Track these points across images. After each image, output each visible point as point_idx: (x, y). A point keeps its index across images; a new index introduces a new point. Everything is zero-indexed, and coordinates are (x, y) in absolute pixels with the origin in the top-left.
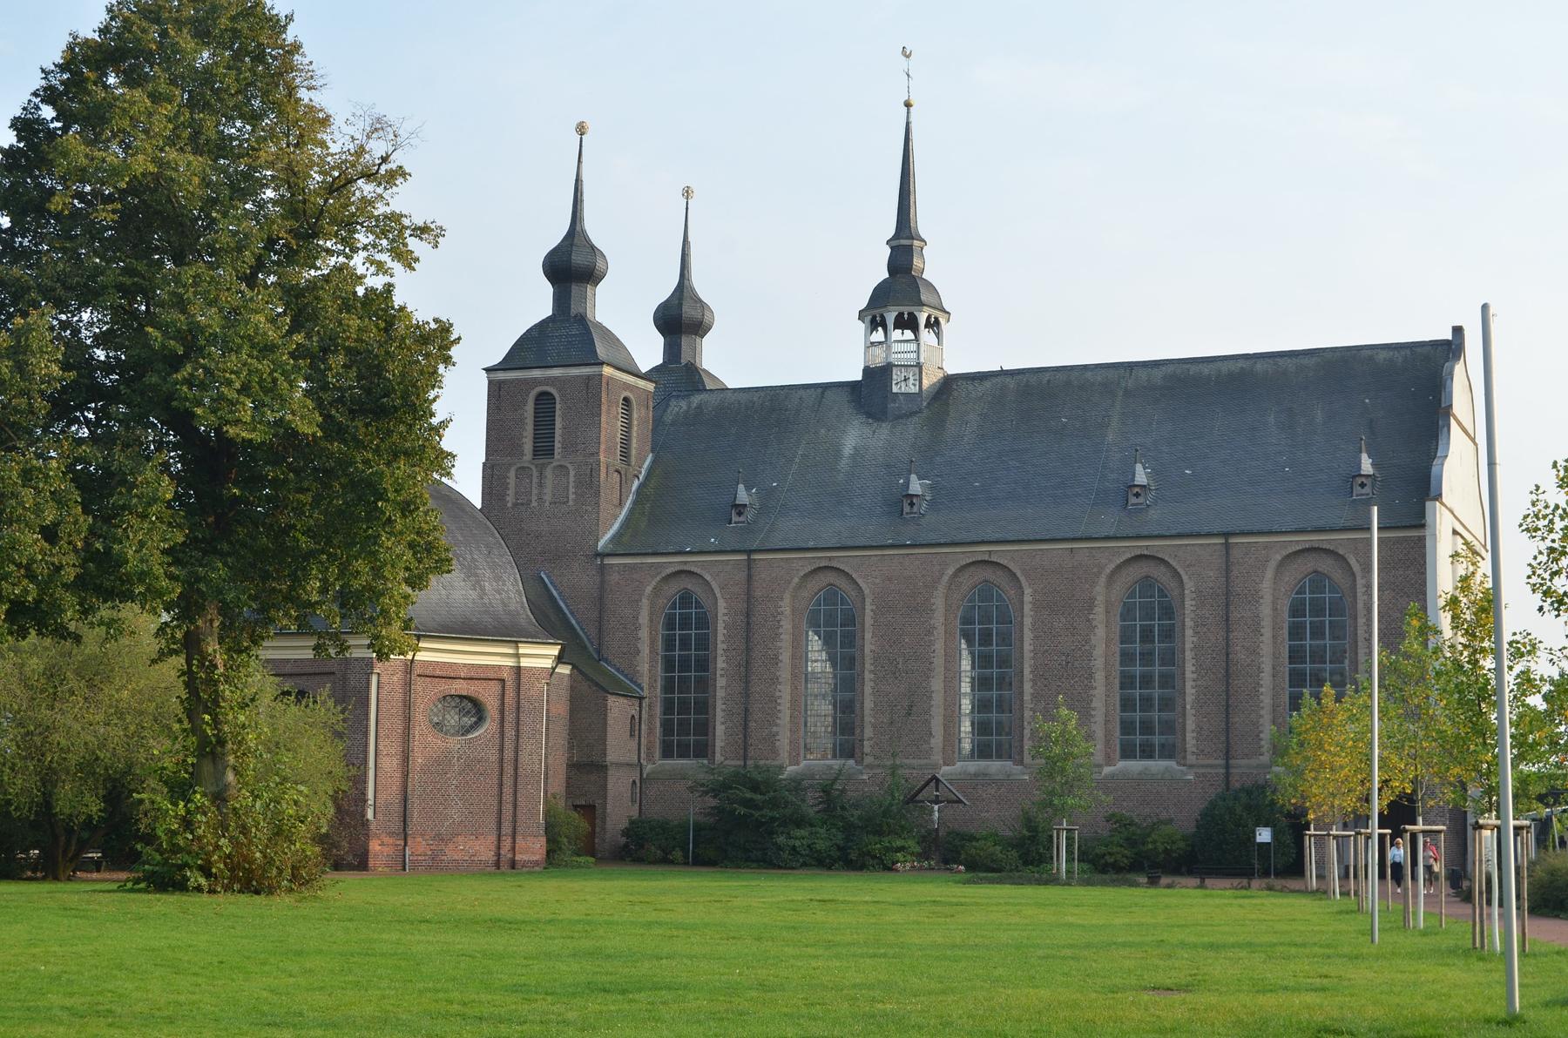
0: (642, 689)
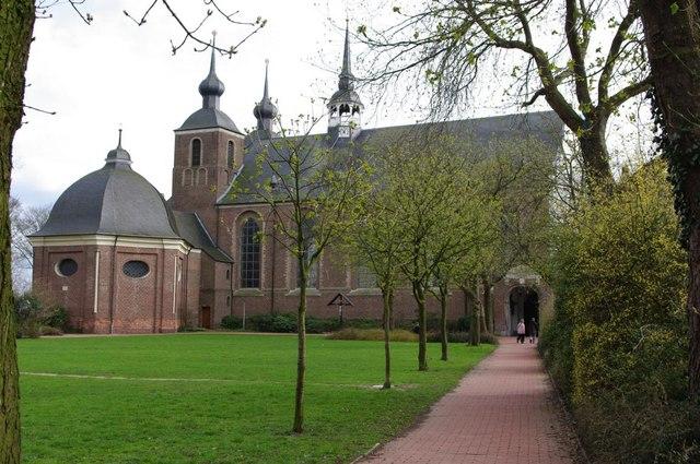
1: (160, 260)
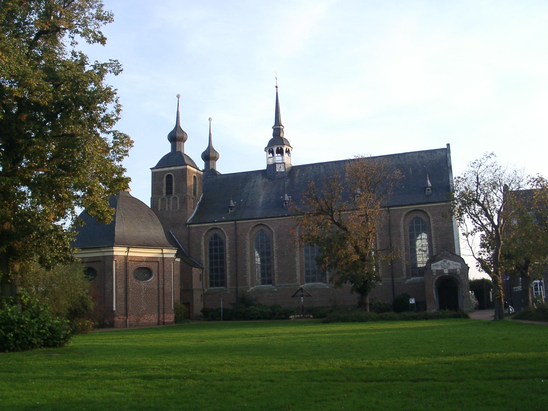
0: (203, 265)
1: (161, 266)
